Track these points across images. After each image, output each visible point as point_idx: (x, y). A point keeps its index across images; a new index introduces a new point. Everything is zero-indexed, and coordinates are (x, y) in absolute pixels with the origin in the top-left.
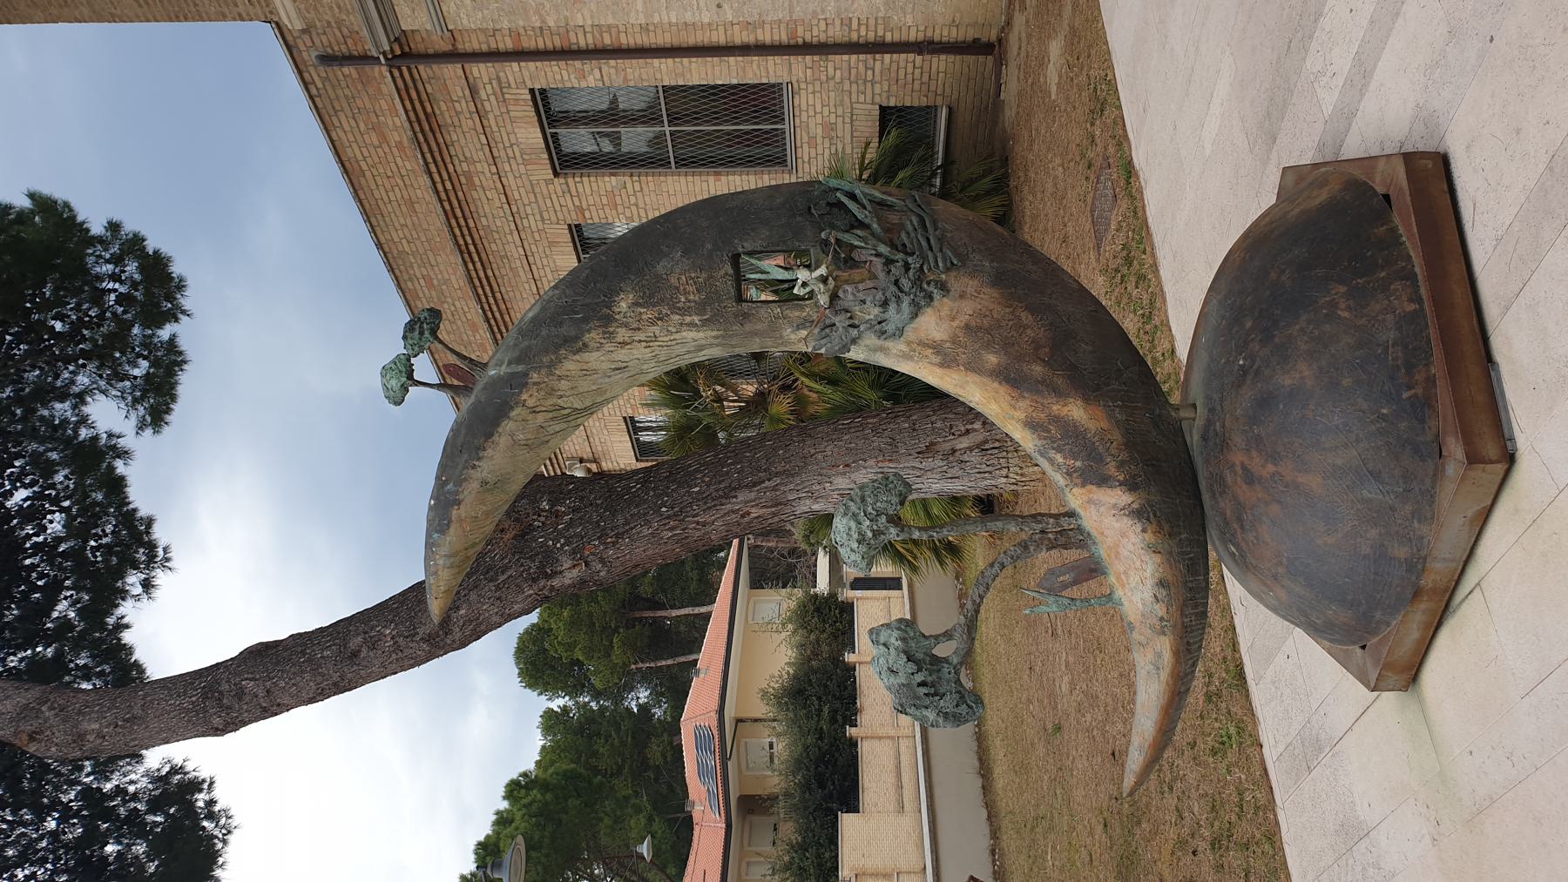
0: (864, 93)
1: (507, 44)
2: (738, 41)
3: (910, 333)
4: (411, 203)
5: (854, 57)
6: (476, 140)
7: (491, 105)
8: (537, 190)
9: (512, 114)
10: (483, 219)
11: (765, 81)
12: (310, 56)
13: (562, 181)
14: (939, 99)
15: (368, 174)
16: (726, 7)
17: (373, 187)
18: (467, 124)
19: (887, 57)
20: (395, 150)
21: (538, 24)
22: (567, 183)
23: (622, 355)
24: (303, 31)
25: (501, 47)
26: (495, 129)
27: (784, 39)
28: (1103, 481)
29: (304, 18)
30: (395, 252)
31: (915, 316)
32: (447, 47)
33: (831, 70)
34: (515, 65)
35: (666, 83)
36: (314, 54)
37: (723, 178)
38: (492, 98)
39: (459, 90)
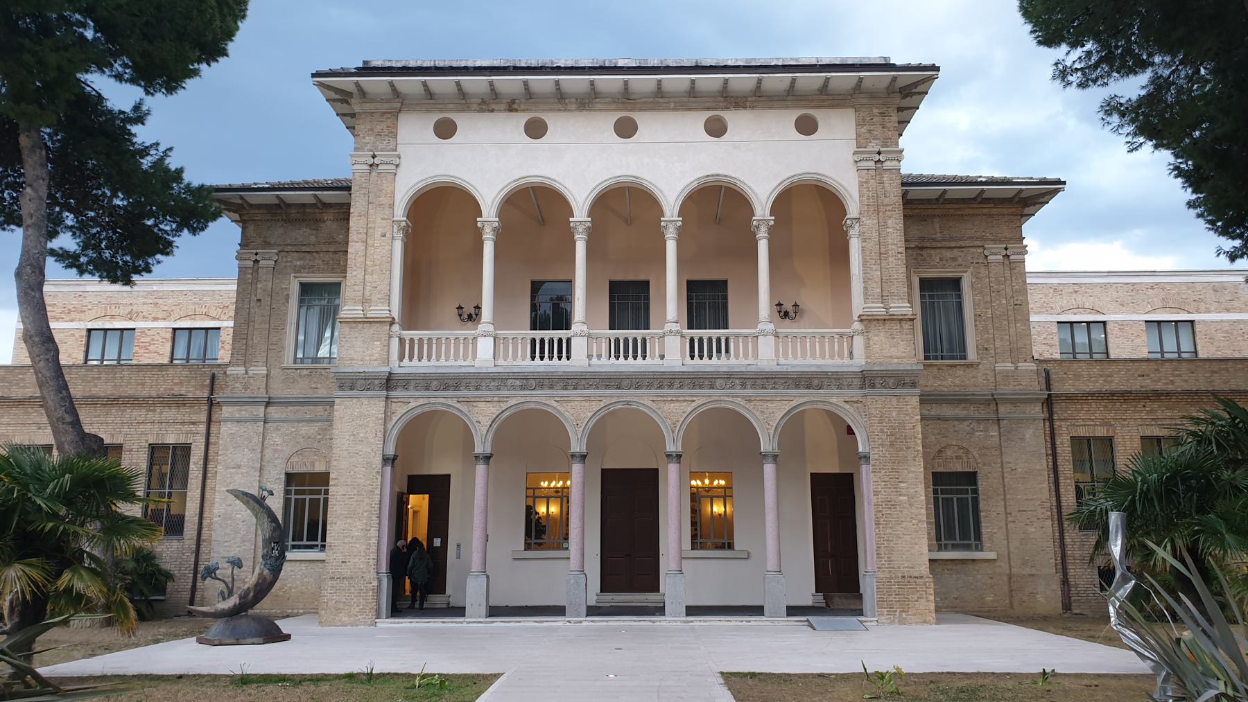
0: (175, 567)
1: (212, 440)
2: (204, 521)
3: (265, 569)
4: (143, 385)
5: (193, 563)
6: (171, 418)
7: (186, 428)
8: (143, 436)
9: (181, 435)
10: (130, 410)
11: (185, 530)
12: (215, 370)
13: (147, 446)
14: (169, 596)
15: (160, 373)
16: (219, 518)
17: (153, 373)
18: (179, 417)
19: (192, 575)
20: (170, 387)
21: (219, 453)
22: (145, 448)
23: (266, 523)
24: (225, 373)
25: (211, 438)
26: (175, 427)
27: (202, 538)
28: (240, 599)
29: (231, 375)
30: (116, 370)
31: (268, 569)
32: (213, 419)
33: (187, 554)
34: (204, 440)
35: (188, 493)
36: (216, 373)
37: (140, 510)
38: (189, 429)
39: (194, 418)
